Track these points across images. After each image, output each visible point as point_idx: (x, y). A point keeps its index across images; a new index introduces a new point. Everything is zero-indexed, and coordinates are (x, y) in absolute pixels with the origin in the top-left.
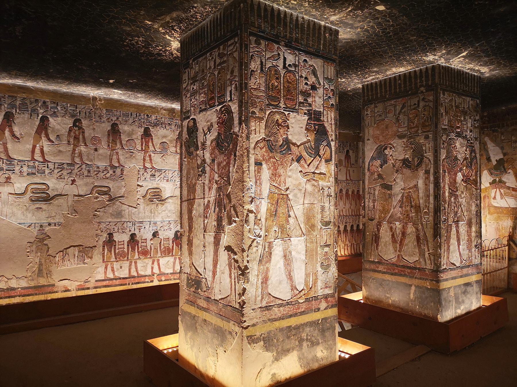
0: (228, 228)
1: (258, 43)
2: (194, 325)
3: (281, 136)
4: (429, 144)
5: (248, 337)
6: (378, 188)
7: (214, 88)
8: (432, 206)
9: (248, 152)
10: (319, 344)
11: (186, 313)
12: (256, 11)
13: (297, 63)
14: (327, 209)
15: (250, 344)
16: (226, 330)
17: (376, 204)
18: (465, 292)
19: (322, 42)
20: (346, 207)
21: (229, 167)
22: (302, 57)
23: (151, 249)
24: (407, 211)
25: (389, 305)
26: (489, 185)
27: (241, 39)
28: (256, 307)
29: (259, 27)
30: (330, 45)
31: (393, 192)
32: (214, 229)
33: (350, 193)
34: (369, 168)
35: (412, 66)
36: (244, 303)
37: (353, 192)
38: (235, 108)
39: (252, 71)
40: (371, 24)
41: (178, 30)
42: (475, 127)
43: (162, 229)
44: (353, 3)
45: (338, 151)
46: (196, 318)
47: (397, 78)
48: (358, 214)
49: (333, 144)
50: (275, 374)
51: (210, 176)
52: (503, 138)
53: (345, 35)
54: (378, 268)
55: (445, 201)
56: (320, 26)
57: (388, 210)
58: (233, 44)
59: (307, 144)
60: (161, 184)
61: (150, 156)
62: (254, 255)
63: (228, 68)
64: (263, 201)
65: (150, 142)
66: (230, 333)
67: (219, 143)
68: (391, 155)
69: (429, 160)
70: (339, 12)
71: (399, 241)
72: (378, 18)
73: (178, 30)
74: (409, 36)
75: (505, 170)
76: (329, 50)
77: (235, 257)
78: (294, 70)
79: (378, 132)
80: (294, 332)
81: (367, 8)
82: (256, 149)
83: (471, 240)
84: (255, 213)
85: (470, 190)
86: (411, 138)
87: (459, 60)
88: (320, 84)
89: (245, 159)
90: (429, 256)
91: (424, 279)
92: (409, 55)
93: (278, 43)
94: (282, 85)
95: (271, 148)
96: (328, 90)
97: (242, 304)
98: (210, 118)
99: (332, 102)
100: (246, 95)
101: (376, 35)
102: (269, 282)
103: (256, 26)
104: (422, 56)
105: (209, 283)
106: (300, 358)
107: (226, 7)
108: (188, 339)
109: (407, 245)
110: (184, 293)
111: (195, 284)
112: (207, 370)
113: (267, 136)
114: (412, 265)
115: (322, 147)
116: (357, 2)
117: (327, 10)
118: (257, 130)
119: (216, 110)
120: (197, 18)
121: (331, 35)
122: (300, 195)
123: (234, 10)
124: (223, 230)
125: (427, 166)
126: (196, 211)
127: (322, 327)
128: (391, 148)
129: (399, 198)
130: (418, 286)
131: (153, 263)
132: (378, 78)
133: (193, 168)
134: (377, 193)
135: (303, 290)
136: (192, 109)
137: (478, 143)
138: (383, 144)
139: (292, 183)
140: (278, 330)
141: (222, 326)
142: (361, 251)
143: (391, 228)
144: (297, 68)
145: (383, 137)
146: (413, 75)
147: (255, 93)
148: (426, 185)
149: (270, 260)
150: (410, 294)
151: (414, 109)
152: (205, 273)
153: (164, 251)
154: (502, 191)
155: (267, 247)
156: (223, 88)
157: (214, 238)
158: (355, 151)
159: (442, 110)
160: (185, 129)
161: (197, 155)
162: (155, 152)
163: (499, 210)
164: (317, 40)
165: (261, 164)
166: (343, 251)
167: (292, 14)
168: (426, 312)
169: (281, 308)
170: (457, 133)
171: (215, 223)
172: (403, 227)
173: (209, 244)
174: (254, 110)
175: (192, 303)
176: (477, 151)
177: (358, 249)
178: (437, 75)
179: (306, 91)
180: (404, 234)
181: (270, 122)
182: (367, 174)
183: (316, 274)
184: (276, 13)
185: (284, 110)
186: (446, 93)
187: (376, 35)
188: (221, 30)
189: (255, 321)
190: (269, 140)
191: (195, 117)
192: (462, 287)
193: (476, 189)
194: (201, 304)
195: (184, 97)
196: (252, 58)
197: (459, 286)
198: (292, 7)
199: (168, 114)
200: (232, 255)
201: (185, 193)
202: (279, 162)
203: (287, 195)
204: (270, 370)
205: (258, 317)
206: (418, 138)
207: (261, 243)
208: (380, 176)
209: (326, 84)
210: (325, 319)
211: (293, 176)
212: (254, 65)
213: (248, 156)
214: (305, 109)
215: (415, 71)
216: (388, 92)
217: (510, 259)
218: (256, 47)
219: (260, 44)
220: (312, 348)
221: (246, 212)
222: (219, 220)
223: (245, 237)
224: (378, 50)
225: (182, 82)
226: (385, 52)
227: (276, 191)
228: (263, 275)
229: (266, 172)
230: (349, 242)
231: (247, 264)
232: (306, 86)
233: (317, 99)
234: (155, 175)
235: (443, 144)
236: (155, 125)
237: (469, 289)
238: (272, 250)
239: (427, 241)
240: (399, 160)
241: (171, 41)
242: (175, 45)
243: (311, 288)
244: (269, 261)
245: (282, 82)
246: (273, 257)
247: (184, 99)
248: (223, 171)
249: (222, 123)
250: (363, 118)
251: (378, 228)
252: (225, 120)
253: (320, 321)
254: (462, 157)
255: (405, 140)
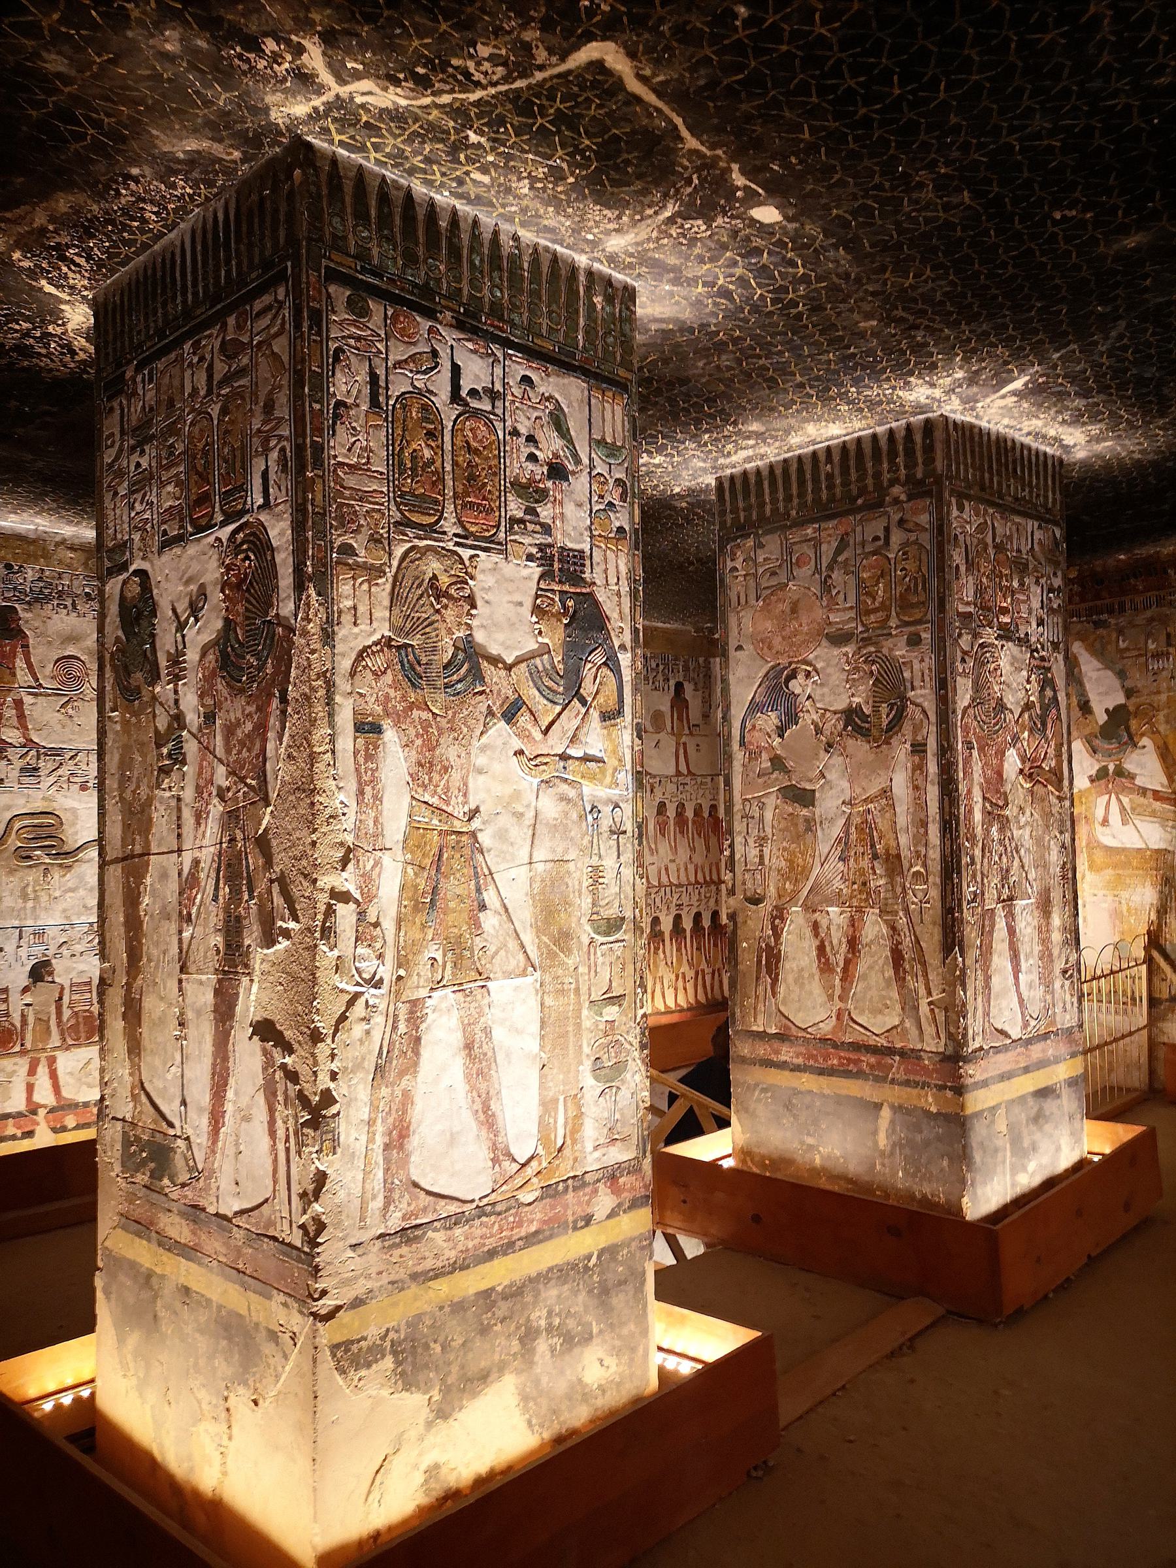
0: (260, 957)
1: (359, 310)
2: (144, 1315)
3: (450, 632)
4: (922, 660)
5: (334, 1348)
6: (772, 801)
7: (208, 465)
8: (935, 854)
9: (330, 686)
10: (591, 1337)
11: (119, 1263)
12: (348, 199)
13: (498, 387)
14: (609, 877)
15: (342, 1371)
16: (257, 1325)
17: (767, 851)
18: (1038, 1119)
19: (582, 322)
20: (674, 858)
21: (265, 741)
22: (515, 366)
23: (24, 1021)
24: (862, 872)
25: (815, 1172)
26: (1087, 784)
27: (297, 292)
28: (365, 1236)
29: (363, 255)
30: (607, 333)
31: (817, 811)
32: (213, 962)
33: (689, 814)
34: (742, 737)
35: (866, 418)
36: (321, 1227)
37: (698, 812)
38: (282, 534)
39: (340, 404)
40: (738, 271)
41: (82, 261)
42: (1051, 611)
43: (65, 952)
44: (677, 191)
45: (647, 678)
46: (154, 1280)
47: (822, 457)
48: (715, 877)
49: (625, 659)
50: (437, 1466)
51: (200, 774)
52: (1122, 645)
53: (659, 305)
54: (777, 1052)
55: (972, 838)
56: (574, 270)
57: (804, 868)
58: (268, 309)
59: (538, 661)
60: (59, 797)
61: (19, 704)
62: (354, 1053)
63: (254, 394)
64: (386, 858)
65: (20, 656)
66: (273, 1336)
67: (228, 658)
68: (809, 697)
69: (924, 712)
70: (634, 223)
71: (838, 965)
72: (758, 252)
73: (82, 261)
74: (856, 316)
75: (1131, 737)
76: (605, 350)
77: (288, 1060)
78: (489, 408)
79: (769, 625)
80: (503, 1308)
81: (725, 214)
82: (357, 677)
83: (1050, 955)
84: (357, 902)
85: (1043, 800)
86: (866, 641)
87: (1002, 402)
88: (578, 461)
89: (319, 710)
90: (932, 1011)
91: (917, 1084)
92: (856, 382)
93: (430, 314)
94: (448, 457)
95: (413, 673)
96: (606, 483)
97: (312, 1229)
98: (195, 567)
99: (621, 519)
100: (318, 487)
101: (755, 309)
102: (414, 1142)
103: (352, 251)
104: (894, 388)
105: (199, 1156)
106: (525, 1398)
107: (245, 182)
108: (129, 1357)
109: (864, 977)
110: (114, 1190)
111: (151, 1158)
112: (192, 1469)
113: (399, 630)
114: (882, 1042)
115: (588, 671)
116: (689, 190)
117: (595, 212)
118: (362, 609)
119: (218, 539)
120: (144, 221)
121: (609, 300)
122: (519, 834)
123: (272, 191)
124: (246, 966)
125: (917, 729)
126: (154, 894)
127: (602, 1278)
128: (808, 675)
129: (836, 830)
130: (900, 1107)
131: (32, 1072)
132: (762, 457)
133: (143, 744)
134: (769, 815)
135: (532, 1158)
136: (137, 537)
137: (1060, 657)
138: (784, 661)
139: (488, 791)
140: (447, 1309)
141: (244, 1312)
142: (727, 994)
143: (816, 926)
144: (499, 404)
145: (784, 638)
146: (867, 449)
147: (351, 481)
148: (916, 788)
149: (416, 1064)
150: (875, 1133)
151: (874, 553)
152: (184, 1118)
153: (75, 1028)
154: (1125, 800)
155: (402, 1017)
156: (238, 465)
157: (217, 992)
158: (701, 685)
159: (958, 558)
160: (113, 609)
161: (154, 698)
162: (36, 689)
163: (1119, 857)
164: (564, 313)
165: (377, 729)
166: (669, 995)
167: (476, 223)
168: (927, 1189)
169: (458, 1231)
170: (1002, 626)
171: (218, 940)
172: (852, 923)
173: (199, 1013)
174: (348, 539)
175: (141, 1227)
176: (1060, 682)
177: (716, 987)
178: (939, 448)
179: (532, 481)
180: (853, 943)
181: (407, 583)
182: (739, 756)
183: (576, 1099)
184: (421, 213)
185: (457, 544)
186: (966, 504)
187: (755, 309)
188: (228, 262)
189: (360, 1288)
190: (406, 646)
191: (145, 566)
192: (1031, 1101)
193: (1060, 799)
194: (172, 1232)
195: (108, 497)
196: (337, 359)
197: (1022, 1099)
198: (478, 197)
199: (86, 564)
200: (277, 1054)
201: (115, 831)
202: (443, 723)
203: (473, 835)
204: (420, 1455)
205: (373, 1271)
206: (887, 644)
207: (382, 1007)
208: (777, 762)
209: (597, 461)
210: (609, 1252)
211: (494, 770)
212: (347, 384)
213: (329, 701)
214: (529, 542)
215: (874, 436)
216: (796, 501)
217: (1153, 1002)
218: (354, 323)
219: (365, 312)
220: (567, 1358)
221: (323, 898)
222: (232, 928)
223: (323, 989)
224: (762, 362)
225: (100, 445)
226: (783, 370)
227: (435, 822)
228: (390, 1120)
229: (395, 757)
230: (691, 965)
231: (332, 1085)
232: (530, 466)
233: (569, 509)
234: (36, 769)
235: (963, 661)
236: (37, 600)
237: (1050, 1105)
238: (423, 1026)
239: (924, 964)
240: (835, 713)
241: (61, 301)
242: (78, 316)
243: (560, 1150)
244: (412, 1067)
245: (448, 446)
246: (425, 1052)
247: (108, 503)
248: (245, 754)
249: (238, 586)
250: (722, 581)
251: (774, 928)
252: (246, 575)
253: (594, 1260)
254: (1018, 703)
255: (849, 649)
